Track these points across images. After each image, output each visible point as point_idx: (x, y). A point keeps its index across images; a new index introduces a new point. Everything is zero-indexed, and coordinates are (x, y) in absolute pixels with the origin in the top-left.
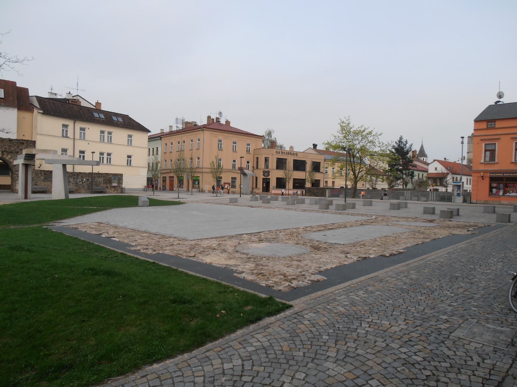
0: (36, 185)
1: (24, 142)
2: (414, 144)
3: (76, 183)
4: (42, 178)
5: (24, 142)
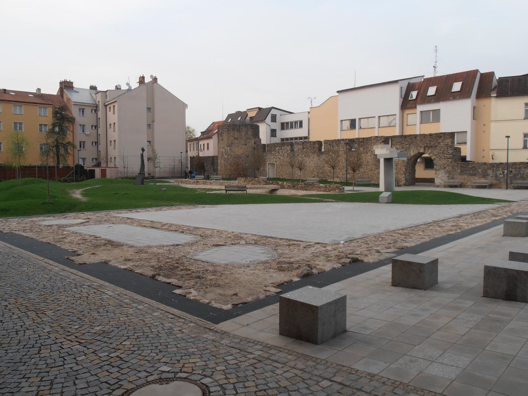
0: (452, 178)
1: (442, 135)
2: (196, 130)
3: (496, 176)
4: (459, 171)
5: (442, 135)
